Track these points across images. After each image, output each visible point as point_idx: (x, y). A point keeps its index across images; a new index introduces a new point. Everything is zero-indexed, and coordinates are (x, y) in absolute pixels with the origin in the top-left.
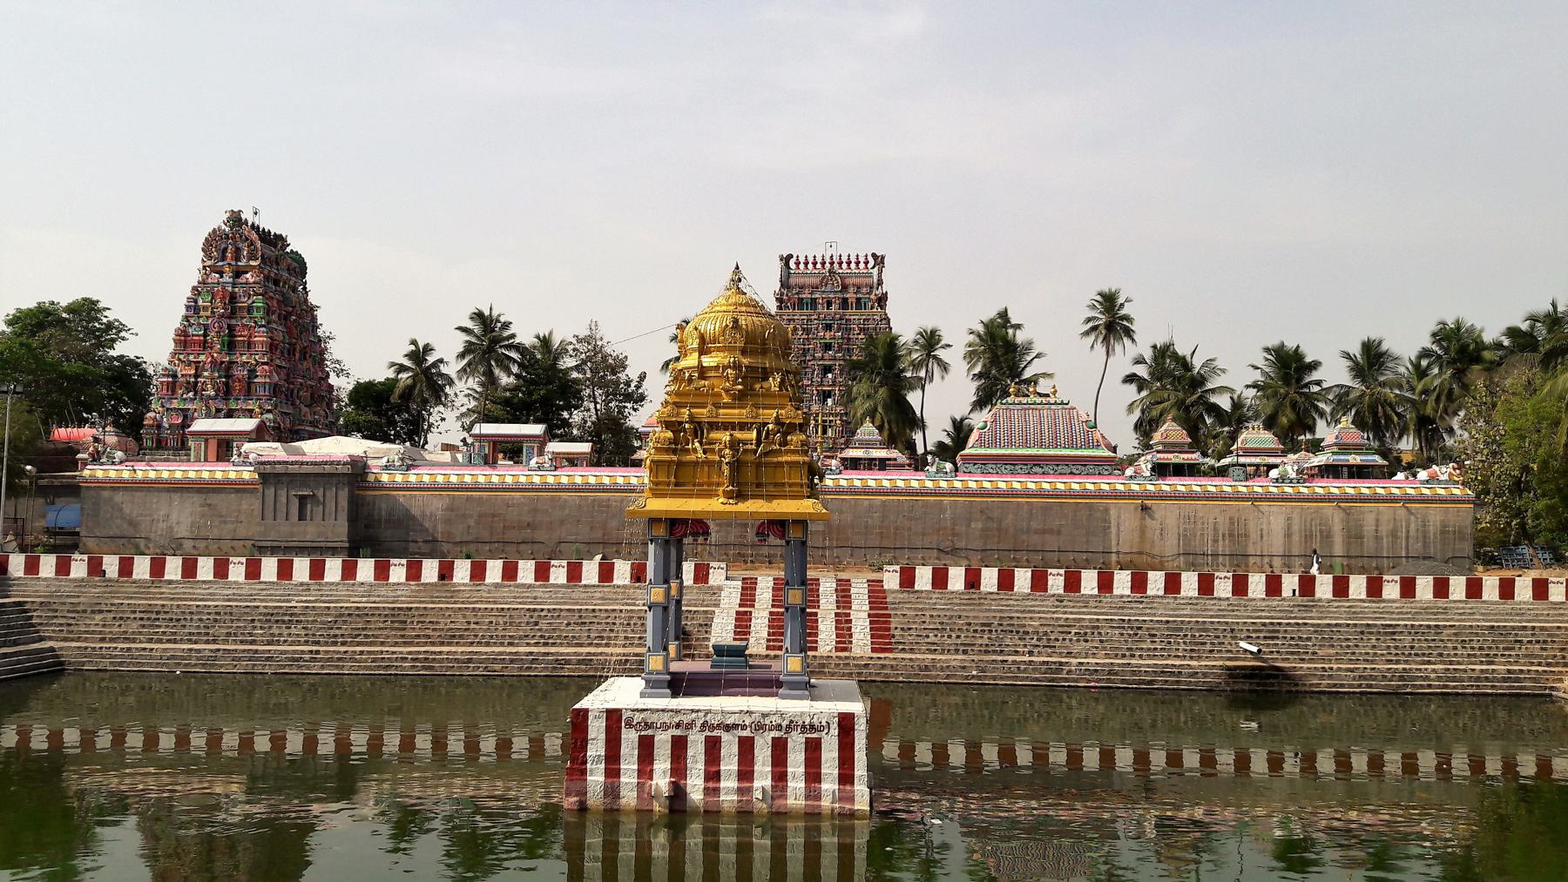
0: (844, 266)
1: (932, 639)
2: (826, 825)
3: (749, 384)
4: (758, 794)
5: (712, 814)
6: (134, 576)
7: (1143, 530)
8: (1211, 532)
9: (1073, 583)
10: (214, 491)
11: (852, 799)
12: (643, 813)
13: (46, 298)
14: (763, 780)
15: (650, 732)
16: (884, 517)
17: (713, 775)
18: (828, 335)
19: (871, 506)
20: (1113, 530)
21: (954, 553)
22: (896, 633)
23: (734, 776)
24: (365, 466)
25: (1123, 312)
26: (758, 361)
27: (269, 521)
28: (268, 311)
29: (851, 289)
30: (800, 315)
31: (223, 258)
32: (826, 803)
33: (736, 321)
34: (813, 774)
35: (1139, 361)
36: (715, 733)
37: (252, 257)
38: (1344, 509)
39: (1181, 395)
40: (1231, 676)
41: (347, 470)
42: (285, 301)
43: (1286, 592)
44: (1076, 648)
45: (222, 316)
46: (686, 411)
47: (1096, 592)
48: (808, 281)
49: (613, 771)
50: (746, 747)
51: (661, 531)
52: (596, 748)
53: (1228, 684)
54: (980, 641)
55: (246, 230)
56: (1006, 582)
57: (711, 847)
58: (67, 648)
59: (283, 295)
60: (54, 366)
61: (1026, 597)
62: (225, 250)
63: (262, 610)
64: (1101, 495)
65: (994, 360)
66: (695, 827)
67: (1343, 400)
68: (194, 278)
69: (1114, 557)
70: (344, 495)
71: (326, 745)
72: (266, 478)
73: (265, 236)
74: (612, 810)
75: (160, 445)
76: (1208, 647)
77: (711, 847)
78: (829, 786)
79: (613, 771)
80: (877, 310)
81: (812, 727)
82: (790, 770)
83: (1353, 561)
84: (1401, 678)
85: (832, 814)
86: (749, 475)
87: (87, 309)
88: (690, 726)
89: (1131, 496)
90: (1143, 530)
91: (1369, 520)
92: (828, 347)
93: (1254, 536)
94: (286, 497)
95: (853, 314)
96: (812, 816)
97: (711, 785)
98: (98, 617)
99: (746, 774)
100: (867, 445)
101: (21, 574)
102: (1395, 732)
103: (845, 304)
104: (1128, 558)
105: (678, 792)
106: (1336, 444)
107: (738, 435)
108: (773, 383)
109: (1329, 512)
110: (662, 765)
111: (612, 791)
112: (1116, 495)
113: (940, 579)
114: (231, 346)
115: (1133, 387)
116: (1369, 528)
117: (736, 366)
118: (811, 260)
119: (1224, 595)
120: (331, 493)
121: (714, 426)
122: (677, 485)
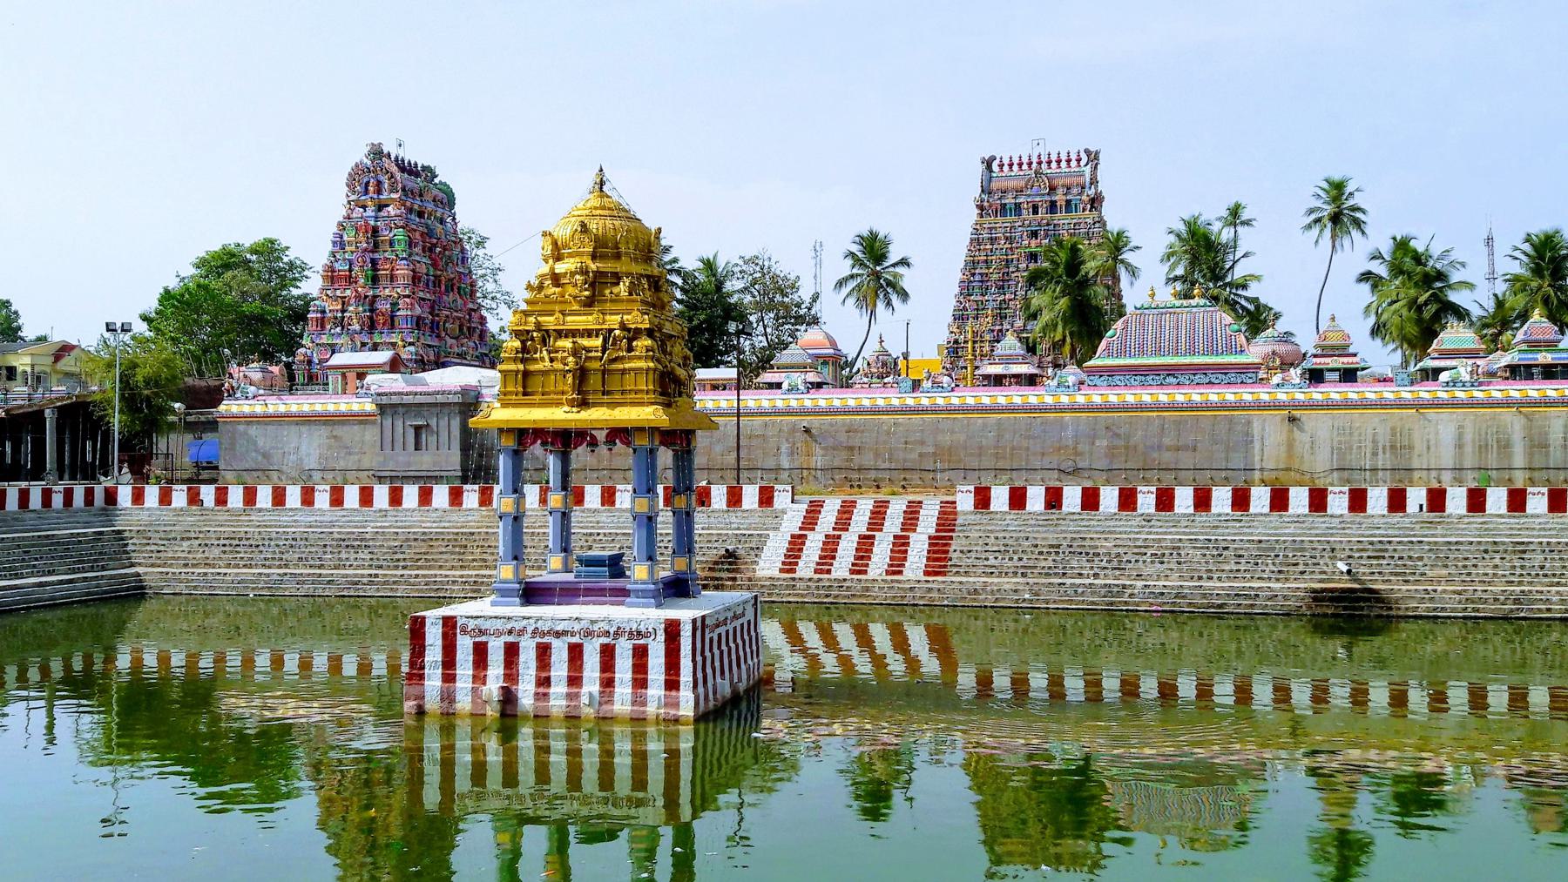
0: (1054, 165)
1: (992, 562)
2: (651, 730)
3: (597, 287)
4: (585, 700)
5: (541, 718)
6: (229, 505)
7: (1290, 445)
8: (1370, 445)
10: (343, 423)
11: (677, 705)
12: (476, 716)
15: (483, 639)
16: (999, 437)
17: (544, 682)
18: (1034, 242)
19: (985, 425)
20: (1257, 446)
22: (954, 556)
23: (564, 682)
24: (479, 395)
25: (1351, 202)
26: (608, 266)
27: (388, 450)
28: (411, 244)
29: (1060, 191)
30: (1002, 222)
31: (366, 192)
32: (651, 709)
33: (583, 225)
34: (640, 682)
35: (1377, 256)
36: (546, 640)
37: (393, 190)
38: (1526, 416)
39: (1413, 292)
40: (1315, 599)
41: (457, 399)
42: (429, 233)
44: (1149, 570)
45: (365, 250)
46: (532, 319)
47: (1191, 510)
48: (1012, 184)
49: (449, 678)
50: (576, 653)
51: (509, 442)
52: (433, 654)
53: (1310, 607)
54: (1043, 564)
55: (386, 162)
58: (148, 573)
59: (427, 226)
60: (234, 307)
61: (1111, 517)
62: (367, 184)
63: (336, 536)
65: (1194, 261)
68: (340, 213)
69: (1257, 475)
70: (456, 423)
71: (178, 660)
72: (382, 408)
74: (448, 714)
75: (312, 379)
76: (1301, 568)
77: (543, 750)
79: (449, 678)
80: (1090, 217)
81: (639, 633)
82: (617, 676)
83: (1536, 474)
84: (1517, 601)
85: (657, 721)
86: (594, 382)
87: (269, 250)
88: (521, 632)
89: (1276, 406)
90: (1290, 445)
92: (1033, 257)
93: (1419, 446)
94: (402, 427)
95: (1061, 218)
97: (541, 690)
98: (185, 544)
100: (1008, 360)
101: (129, 504)
102: (1524, 665)
103: (1053, 207)
104: (1274, 475)
105: (508, 698)
106: (1524, 341)
107: (585, 342)
108: (622, 289)
109: (1509, 419)
110: (496, 670)
111: (448, 697)
112: (1260, 406)
114: (375, 280)
115: (1366, 287)
117: (584, 271)
118: (1064, 157)
119: (1339, 512)
120: (444, 422)
121: (560, 334)
122: (525, 394)
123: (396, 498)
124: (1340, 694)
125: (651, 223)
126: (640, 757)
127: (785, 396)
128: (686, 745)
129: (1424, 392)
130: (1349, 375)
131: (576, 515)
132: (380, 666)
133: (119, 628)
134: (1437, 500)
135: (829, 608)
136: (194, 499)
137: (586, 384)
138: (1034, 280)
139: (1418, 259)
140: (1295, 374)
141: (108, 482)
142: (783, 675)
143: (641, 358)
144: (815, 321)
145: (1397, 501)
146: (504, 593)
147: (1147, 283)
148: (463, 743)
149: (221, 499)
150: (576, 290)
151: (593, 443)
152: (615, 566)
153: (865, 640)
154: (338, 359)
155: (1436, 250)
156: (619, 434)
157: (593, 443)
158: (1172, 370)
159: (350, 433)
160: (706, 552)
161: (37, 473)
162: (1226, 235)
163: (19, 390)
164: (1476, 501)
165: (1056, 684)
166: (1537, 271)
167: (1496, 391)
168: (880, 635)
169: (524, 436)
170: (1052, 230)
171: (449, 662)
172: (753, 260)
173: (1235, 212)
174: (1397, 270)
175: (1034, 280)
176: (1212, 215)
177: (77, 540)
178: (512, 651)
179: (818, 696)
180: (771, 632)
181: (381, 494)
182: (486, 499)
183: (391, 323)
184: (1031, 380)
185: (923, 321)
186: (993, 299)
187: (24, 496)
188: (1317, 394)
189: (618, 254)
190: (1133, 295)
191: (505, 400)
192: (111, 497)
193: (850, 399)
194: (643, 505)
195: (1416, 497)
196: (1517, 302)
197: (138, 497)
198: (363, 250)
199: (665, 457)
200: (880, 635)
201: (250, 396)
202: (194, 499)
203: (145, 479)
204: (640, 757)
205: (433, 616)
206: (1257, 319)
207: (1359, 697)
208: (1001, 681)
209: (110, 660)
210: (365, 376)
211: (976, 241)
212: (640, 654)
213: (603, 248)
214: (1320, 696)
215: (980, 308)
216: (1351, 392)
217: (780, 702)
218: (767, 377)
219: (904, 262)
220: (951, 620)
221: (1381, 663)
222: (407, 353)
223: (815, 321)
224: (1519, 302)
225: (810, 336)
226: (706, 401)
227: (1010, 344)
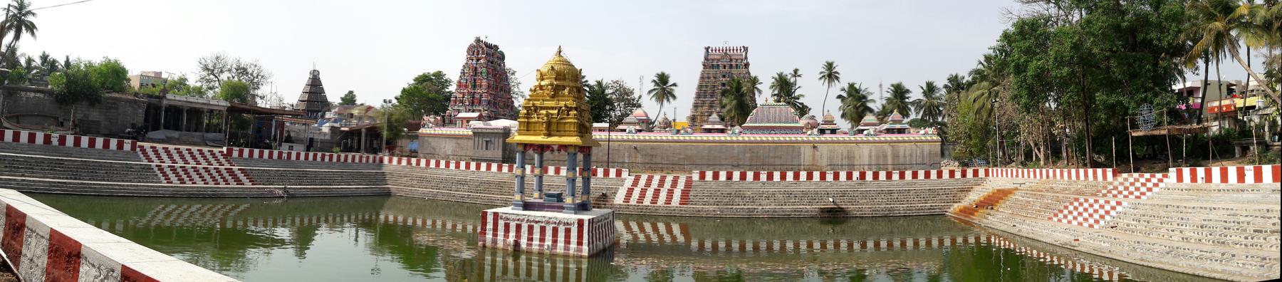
3: (556, 91)
5: (529, 253)
9: (770, 177)
12: (505, 250)
13: (426, 71)
14: (548, 242)
17: (530, 239)
21: (737, 166)
30: (712, 71)
32: (571, 252)
34: (567, 241)
42: (495, 69)
43: (854, 178)
49: (495, 235)
50: (543, 230)
51: (521, 148)
52: (490, 226)
56: (743, 177)
57: (529, 264)
64: (797, 142)
65: (781, 89)
66: (523, 257)
67: (917, 104)
71: (400, 219)
73: (489, 46)
75: (451, 122)
77: (529, 264)
78: (573, 245)
79: (495, 235)
80: (744, 71)
86: (554, 127)
87: (439, 75)
91: (902, 150)
92: (724, 85)
94: (482, 141)
95: (734, 71)
96: (566, 257)
99: (542, 239)
100: (714, 123)
105: (517, 244)
108: (566, 91)
110: (512, 234)
111: (495, 242)
112: (804, 142)
113: (716, 176)
114: (475, 87)
116: (901, 154)
117: (551, 85)
121: (542, 108)
123: (478, 167)
124: (830, 246)
125: (578, 67)
126: (566, 270)
127: (627, 134)
128: (584, 266)
129: (859, 137)
130: (833, 131)
131: (545, 178)
132: (470, 228)
133: (381, 207)
134: (863, 176)
135: (642, 216)
136: (409, 163)
137: (550, 129)
138: (724, 93)
139: (857, 91)
140: (815, 131)
141: (380, 155)
142: (623, 241)
143: (572, 119)
144: (640, 106)
145: (849, 176)
146: (516, 205)
147: (765, 96)
148: (499, 259)
149: (418, 163)
150: (549, 91)
151: (552, 151)
152: (559, 197)
153: (656, 229)
154: (460, 115)
155: (863, 88)
156: (563, 147)
157: (552, 151)
158: (773, 129)
159: (462, 142)
160: (595, 194)
161: (358, 150)
162: (792, 80)
163: (354, 121)
164: (876, 176)
165: (729, 245)
166: (895, 97)
167: (883, 137)
168: (661, 227)
169: (526, 146)
170: (731, 75)
171: (495, 229)
172: (616, 82)
173: (796, 71)
174: (850, 94)
175: (724, 93)
176: (788, 72)
177: (370, 174)
178: (519, 227)
179: (636, 250)
180: (619, 225)
181: (473, 165)
182: (511, 170)
183: (480, 103)
184: (722, 131)
185: (682, 107)
186: (708, 99)
187: (354, 158)
188: (823, 138)
189: (565, 78)
190: (760, 100)
191: (520, 132)
192: (381, 160)
193: (652, 136)
194: (571, 175)
195: (856, 175)
196: (889, 107)
197: (390, 161)
198: (471, 75)
199: (580, 156)
200: (661, 227)
201: (430, 127)
202: (409, 163)
203: (393, 155)
204: (566, 270)
205: (490, 211)
206: (803, 110)
207: (837, 245)
208: (708, 245)
209: (378, 215)
210: (470, 122)
211: (702, 78)
212: (568, 231)
213: (559, 76)
214: (824, 246)
215: (704, 103)
216: (834, 137)
217: (623, 251)
218: (621, 127)
219: (674, 85)
220: (690, 222)
221: (843, 232)
222: (484, 114)
223: (640, 106)
224: (890, 107)
225: (637, 112)
226: (596, 135)
227: (715, 117)
